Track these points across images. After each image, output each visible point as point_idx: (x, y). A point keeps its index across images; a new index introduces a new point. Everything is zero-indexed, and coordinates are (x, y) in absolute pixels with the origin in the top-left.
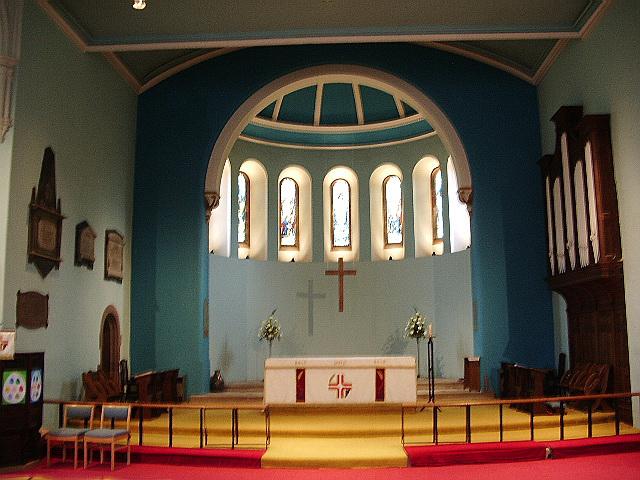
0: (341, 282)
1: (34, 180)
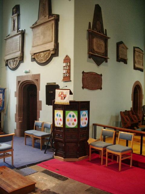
1: (90, 18)
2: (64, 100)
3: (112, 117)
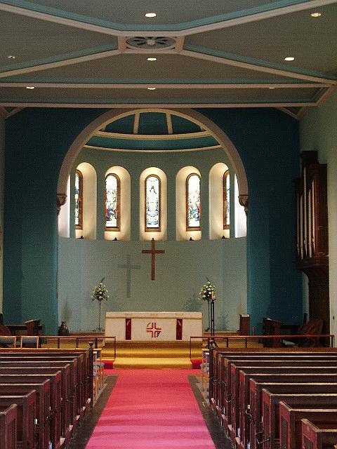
0: (153, 259)
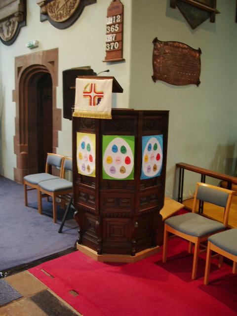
2: (96, 106)
3: (219, 147)
